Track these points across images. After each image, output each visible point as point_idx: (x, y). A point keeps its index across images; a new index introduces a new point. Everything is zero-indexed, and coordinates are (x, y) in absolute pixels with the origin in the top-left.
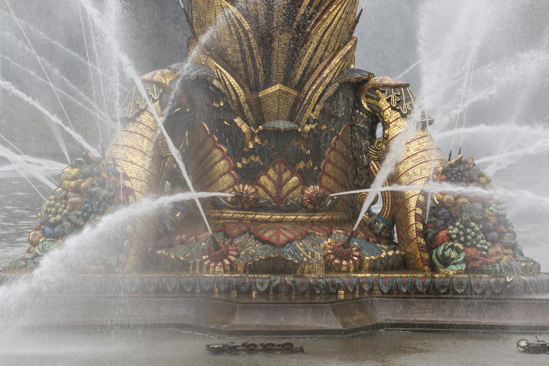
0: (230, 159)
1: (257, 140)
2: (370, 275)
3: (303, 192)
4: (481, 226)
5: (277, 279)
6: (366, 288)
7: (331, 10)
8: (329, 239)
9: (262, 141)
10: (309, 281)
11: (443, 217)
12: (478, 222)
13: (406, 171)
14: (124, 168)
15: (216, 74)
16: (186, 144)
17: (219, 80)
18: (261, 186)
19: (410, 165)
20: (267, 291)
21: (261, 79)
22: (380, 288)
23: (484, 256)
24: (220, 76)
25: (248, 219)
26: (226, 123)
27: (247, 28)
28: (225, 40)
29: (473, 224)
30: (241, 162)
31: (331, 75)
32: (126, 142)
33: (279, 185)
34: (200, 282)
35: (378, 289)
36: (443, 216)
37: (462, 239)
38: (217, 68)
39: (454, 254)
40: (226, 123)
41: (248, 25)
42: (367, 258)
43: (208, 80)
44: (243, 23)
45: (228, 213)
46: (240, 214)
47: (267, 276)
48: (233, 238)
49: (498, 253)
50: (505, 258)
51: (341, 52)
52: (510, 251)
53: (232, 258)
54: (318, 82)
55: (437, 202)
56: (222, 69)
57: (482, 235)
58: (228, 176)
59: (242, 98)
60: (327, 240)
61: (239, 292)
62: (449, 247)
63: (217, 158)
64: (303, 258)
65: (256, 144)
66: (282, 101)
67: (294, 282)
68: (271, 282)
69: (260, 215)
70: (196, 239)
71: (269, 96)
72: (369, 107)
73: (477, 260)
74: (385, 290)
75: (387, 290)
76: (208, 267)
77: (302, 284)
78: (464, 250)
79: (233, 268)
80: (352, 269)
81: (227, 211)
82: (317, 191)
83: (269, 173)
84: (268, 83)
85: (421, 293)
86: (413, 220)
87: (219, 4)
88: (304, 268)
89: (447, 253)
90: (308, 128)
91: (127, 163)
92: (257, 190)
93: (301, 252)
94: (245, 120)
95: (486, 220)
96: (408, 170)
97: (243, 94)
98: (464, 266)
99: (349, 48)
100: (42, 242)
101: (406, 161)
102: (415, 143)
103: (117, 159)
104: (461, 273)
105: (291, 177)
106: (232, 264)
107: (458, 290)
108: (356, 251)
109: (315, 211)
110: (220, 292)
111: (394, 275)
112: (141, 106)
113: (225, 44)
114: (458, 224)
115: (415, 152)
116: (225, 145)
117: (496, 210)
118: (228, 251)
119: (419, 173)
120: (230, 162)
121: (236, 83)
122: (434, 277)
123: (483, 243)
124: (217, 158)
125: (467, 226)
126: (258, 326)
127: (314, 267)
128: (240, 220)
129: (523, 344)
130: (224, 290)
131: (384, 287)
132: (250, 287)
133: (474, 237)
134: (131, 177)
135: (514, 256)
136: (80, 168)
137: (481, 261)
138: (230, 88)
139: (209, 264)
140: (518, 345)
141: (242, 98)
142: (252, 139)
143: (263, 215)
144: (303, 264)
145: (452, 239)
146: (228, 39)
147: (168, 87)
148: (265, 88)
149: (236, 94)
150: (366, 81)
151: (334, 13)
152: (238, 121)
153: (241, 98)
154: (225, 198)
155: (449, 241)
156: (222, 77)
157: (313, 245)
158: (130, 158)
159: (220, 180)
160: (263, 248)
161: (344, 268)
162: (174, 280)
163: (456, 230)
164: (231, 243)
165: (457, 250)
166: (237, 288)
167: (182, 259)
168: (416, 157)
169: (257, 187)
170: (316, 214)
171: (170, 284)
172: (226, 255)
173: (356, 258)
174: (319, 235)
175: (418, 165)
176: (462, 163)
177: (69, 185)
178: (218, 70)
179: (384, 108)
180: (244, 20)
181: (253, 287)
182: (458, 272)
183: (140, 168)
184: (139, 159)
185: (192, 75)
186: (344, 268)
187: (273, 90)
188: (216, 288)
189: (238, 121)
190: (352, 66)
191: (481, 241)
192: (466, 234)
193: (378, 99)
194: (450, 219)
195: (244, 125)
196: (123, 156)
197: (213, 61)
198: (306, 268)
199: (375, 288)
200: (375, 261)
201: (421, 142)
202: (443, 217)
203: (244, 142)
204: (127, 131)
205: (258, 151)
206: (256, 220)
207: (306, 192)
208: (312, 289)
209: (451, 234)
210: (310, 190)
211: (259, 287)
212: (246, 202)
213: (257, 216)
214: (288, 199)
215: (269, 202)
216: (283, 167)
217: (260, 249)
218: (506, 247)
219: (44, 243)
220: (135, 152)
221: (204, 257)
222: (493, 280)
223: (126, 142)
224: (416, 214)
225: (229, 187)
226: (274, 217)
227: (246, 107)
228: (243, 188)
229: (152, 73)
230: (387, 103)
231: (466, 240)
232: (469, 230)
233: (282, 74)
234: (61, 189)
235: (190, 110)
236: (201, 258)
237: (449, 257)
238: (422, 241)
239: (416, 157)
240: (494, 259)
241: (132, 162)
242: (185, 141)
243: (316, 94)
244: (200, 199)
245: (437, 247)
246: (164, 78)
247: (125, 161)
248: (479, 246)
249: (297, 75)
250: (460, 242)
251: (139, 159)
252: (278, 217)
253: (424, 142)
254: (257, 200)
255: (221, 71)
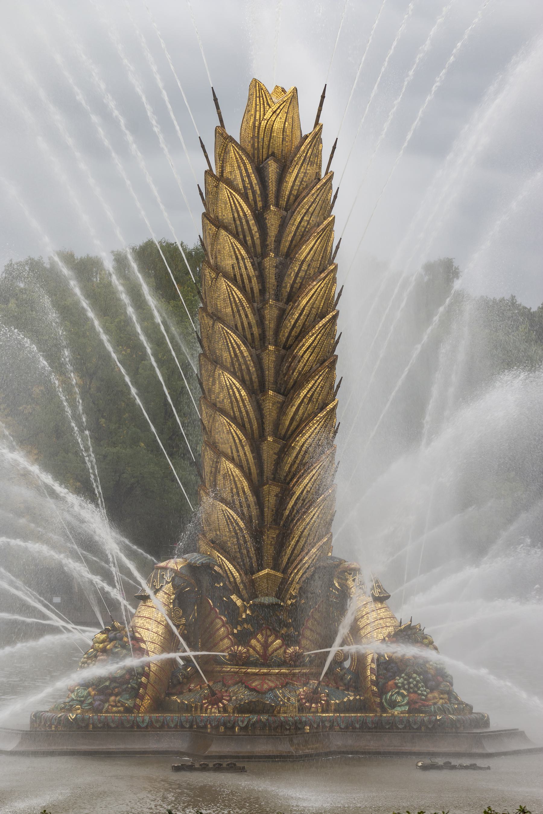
0: (228, 627)
1: (248, 612)
2: (333, 715)
3: (285, 652)
4: (422, 677)
5: (255, 718)
6: (327, 724)
7: (309, 512)
8: (305, 688)
9: (252, 613)
10: (280, 719)
11: (392, 670)
12: (419, 674)
13: (365, 635)
14: (142, 634)
15: (218, 561)
16: (195, 615)
17: (220, 566)
18: (251, 647)
19: (369, 630)
20: (246, 727)
21: (255, 565)
22: (338, 725)
23: (423, 700)
24: (221, 563)
25: (242, 672)
26: (225, 599)
27: (242, 526)
28: (226, 536)
29: (415, 675)
30: (236, 629)
31: (310, 561)
32: (144, 614)
33: (266, 646)
34: (196, 719)
35: (337, 725)
36: (392, 669)
37: (406, 687)
38: (219, 557)
39: (399, 699)
40: (225, 599)
41: (243, 524)
42: (333, 702)
43: (210, 566)
44: (239, 523)
45: (226, 668)
46: (235, 668)
47: (248, 715)
48: (229, 687)
49: (434, 698)
50: (441, 701)
51: (319, 544)
52: (446, 696)
53: (225, 702)
54: (299, 566)
55: (387, 659)
56: (223, 558)
57: (423, 684)
58: (227, 640)
59: (238, 580)
60: (303, 688)
61: (226, 728)
62: (396, 693)
63: (219, 626)
64: (280, 702)
65: (247, 615)
66: (270, 582)
67: (267, 720)
68: (250, 720)
69: (251, 669)
70: (201, 688)
71: (261, 578)
72: (339, 586)
73: (417, 703)
74: (343, 726)
75: (344, 726)
76: (207, 709)
77: (275, 722)
78: (408, 695)
79: (225, 710)
80: (320, 710)
81: (226, 667)
82: (296, 651)
83: (258, 637)
84: (261, 567)
85: (369, 728)
86: (369, 673)
87: (221, 508)
88: (280, 710)
89: (394, 698)
90: (289, 602)
91: (144, 630)
92: (248, 650)
93: (279, 697)
94: (240, 596)
95: (426, 672)
96: (367, 634)
97: (239, 576)
98: (407, 708)
99: (325, 540)
100: (78, 689)
101: (366, 627)
102: (374, 613)
103: (137, 627)
104: (403, 713)
105: (274, 641)
106: (225, 706)
107: (399, 726)
108: (324, 696)
109: (296, 666)
110: (212, 727)
111: (351, 715)
112: (157, 587)
113: (226, 538)
114: (403, 675)
115: (374, 620)
116: (225, 616)
117: (435, 665)
118: (223, 696)
119: (375, 636)
120: (228, 629)
121: (233, 568)
122: (382, 716)
123: (422, 690)
124: (218, 626)
125: (410, 677)
126: (228, 752)
127: (289, 709)
128: (237, 672)
129: (420, 764)
130: (215, 726)
131: (341, 723)
132: (234, 723)
133: (416, 686)
134: (147, 641)
135: (449, 699)
136: (108, 634)
137: (420, 704)
138: (229, 572)
139: (207, 706)
140: (417, 765)
141: (238, 580)
142: (245, 611)
143: (253, 669)
144: (279, 706)
145: (399, 688)
146: (227, 534)
147: (179, 572)
148: (259, 571)
149: (233, 577)
150: (338, 566)
151: (312, 514)
152: (234, 597)
153: (238, 580)
154: (224, 656)
155: (396, 689)
156: (223, 563)
157: (290, 692)
158: (147, 626)
159: (221, 643)
160: (250, 694)
161: (313, 710)
162: (175, 719)
163: (401, 680)
164: (226, 691)
165: (403, 696)
166: (224, 724)
167: (186, 702)
168: (374, 624)
169: (249, 648)
170: (296, 668)
171: (172, 721)
172: (220, 700)
173: (323, 702)
174: (297, 685)
175: (375, 630)
176: (411, 629)
177: (98, 647)
178: (220, 559)
179: (351, 587)
180: (240, 520)
181: (236, 723)
182: (402, 712)
183: (154, 634)
184: (154, 627)
185: (198, 562)
186: (313, 710)
187: (263, 574)
188: (209, 724)
189: (234, 597)
190: (330, 554)
191: (422, 689)
192: (409, 683)
193: (347, 580)
194: (398, 672)
195: (239, 601)
196: (142, 625)
197: (216, 552)
198: (282, 710)
199: (335, 724)
200: (339, 704)
201: (379, 612)
202: (392, 670)
203: (238, 613)
204: (146, 606)
205: (248, 620)
206: (248, 673)
207: (288, 651)
208: (282, 725)
209: (398, 683)
210: (290, 650)
211: (240, 723)
212: (240, 659)
213: (249, 670)
214: (273, 656)
215: (257, 659)
216: (269, 633)
217: (247, 695)
218: (442, 692)
219: (79, 691)
220: (151, 622)
221: (204, 702)
222: (426, 719)
223: (144, 614)
224: (371, 668)
225: (227, 648)
226: (262, 671)
227: (241, 586)
228: (238, 648)
229: (167, 561)
230: (353, 583)
231: (410, 688)
232: (411, 680)
233: (272, 561)
234: (92, 650)
235: (198, 589)
236: (202, 702)
237: (395, 701)
238: (375, 688)
239: (374, 624)
240: (430, 703)
241: (148, 629)
242: (195, 613)
243: (297, 577)
244: (195, 657)
245: (387, 693)
246: (176, 565)
247: (143, 628)
248: (420, 692)
249: (284, 562)
250: (405, 689)
251: (154, 627)
252: (265, 671)
253: (381, 613)
254: (248, 657)
255: (221, 559)
